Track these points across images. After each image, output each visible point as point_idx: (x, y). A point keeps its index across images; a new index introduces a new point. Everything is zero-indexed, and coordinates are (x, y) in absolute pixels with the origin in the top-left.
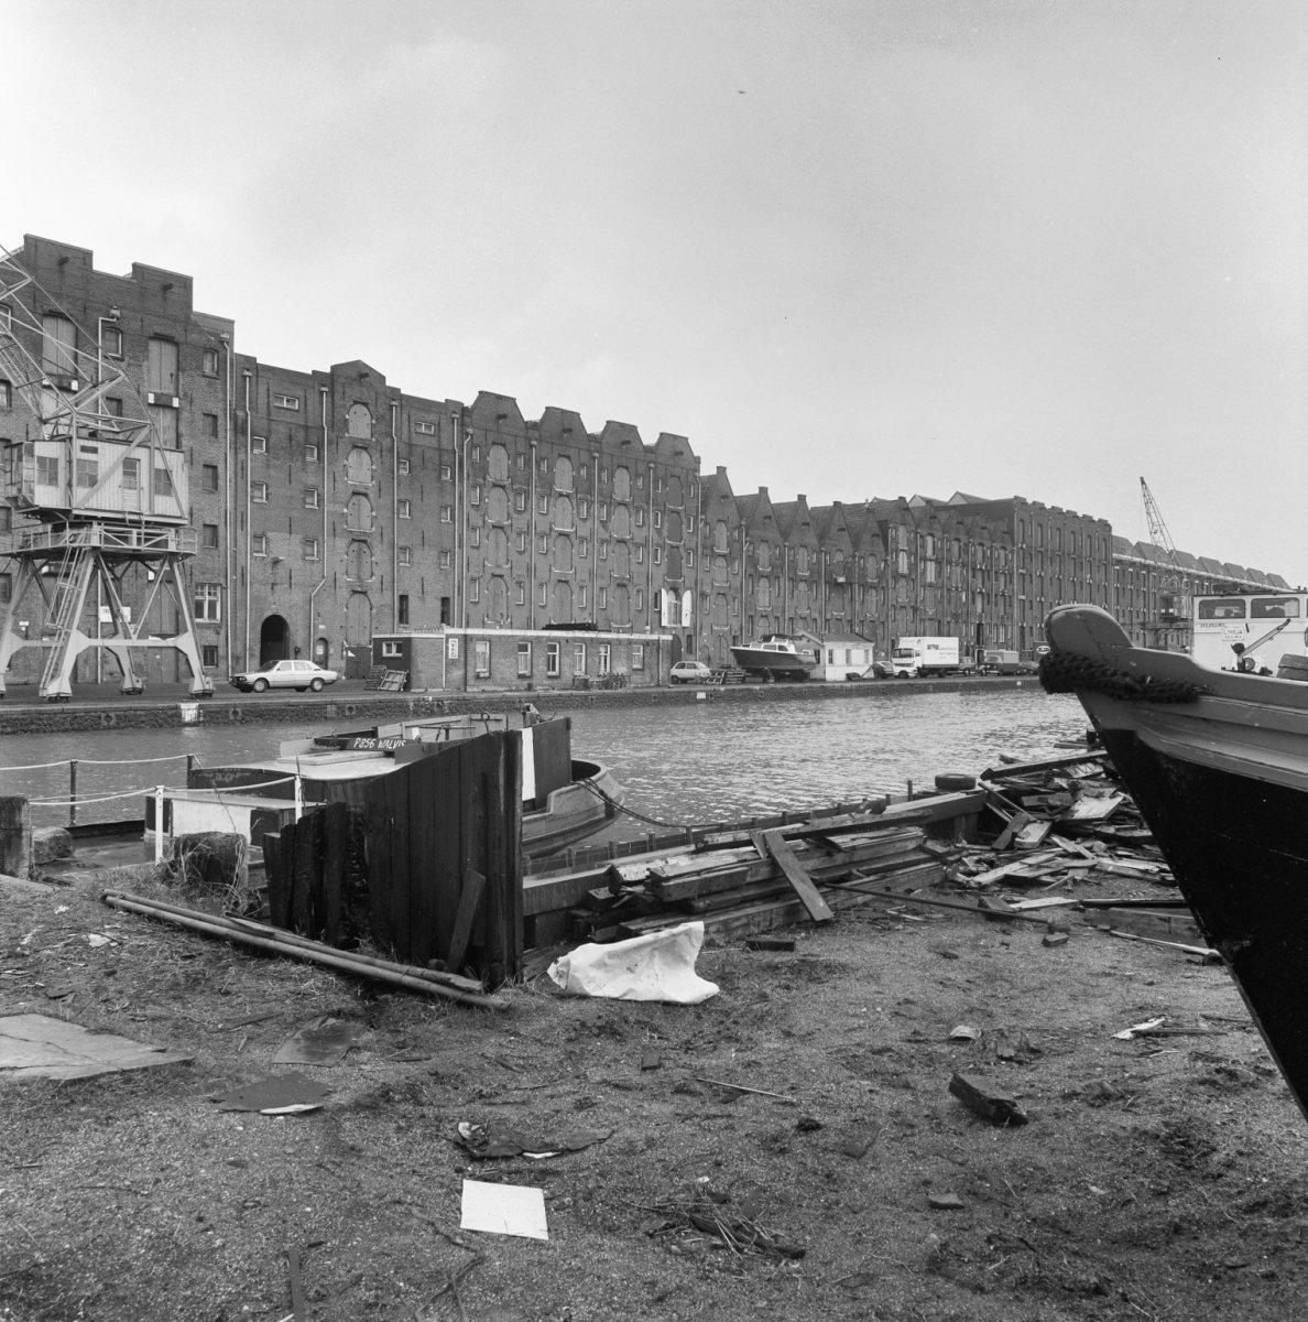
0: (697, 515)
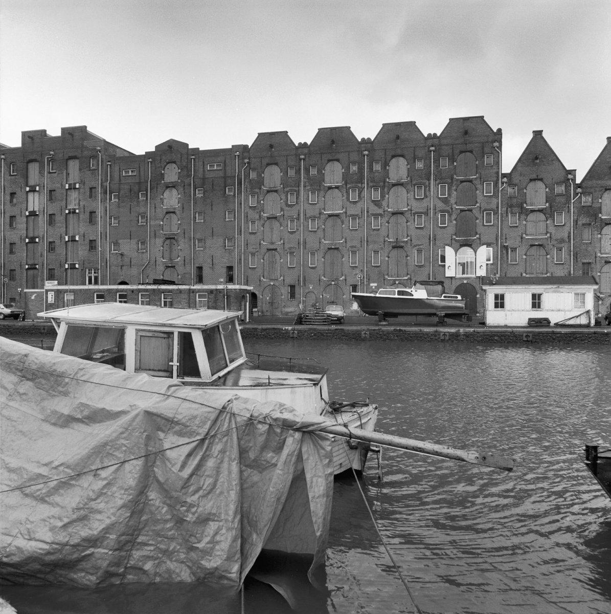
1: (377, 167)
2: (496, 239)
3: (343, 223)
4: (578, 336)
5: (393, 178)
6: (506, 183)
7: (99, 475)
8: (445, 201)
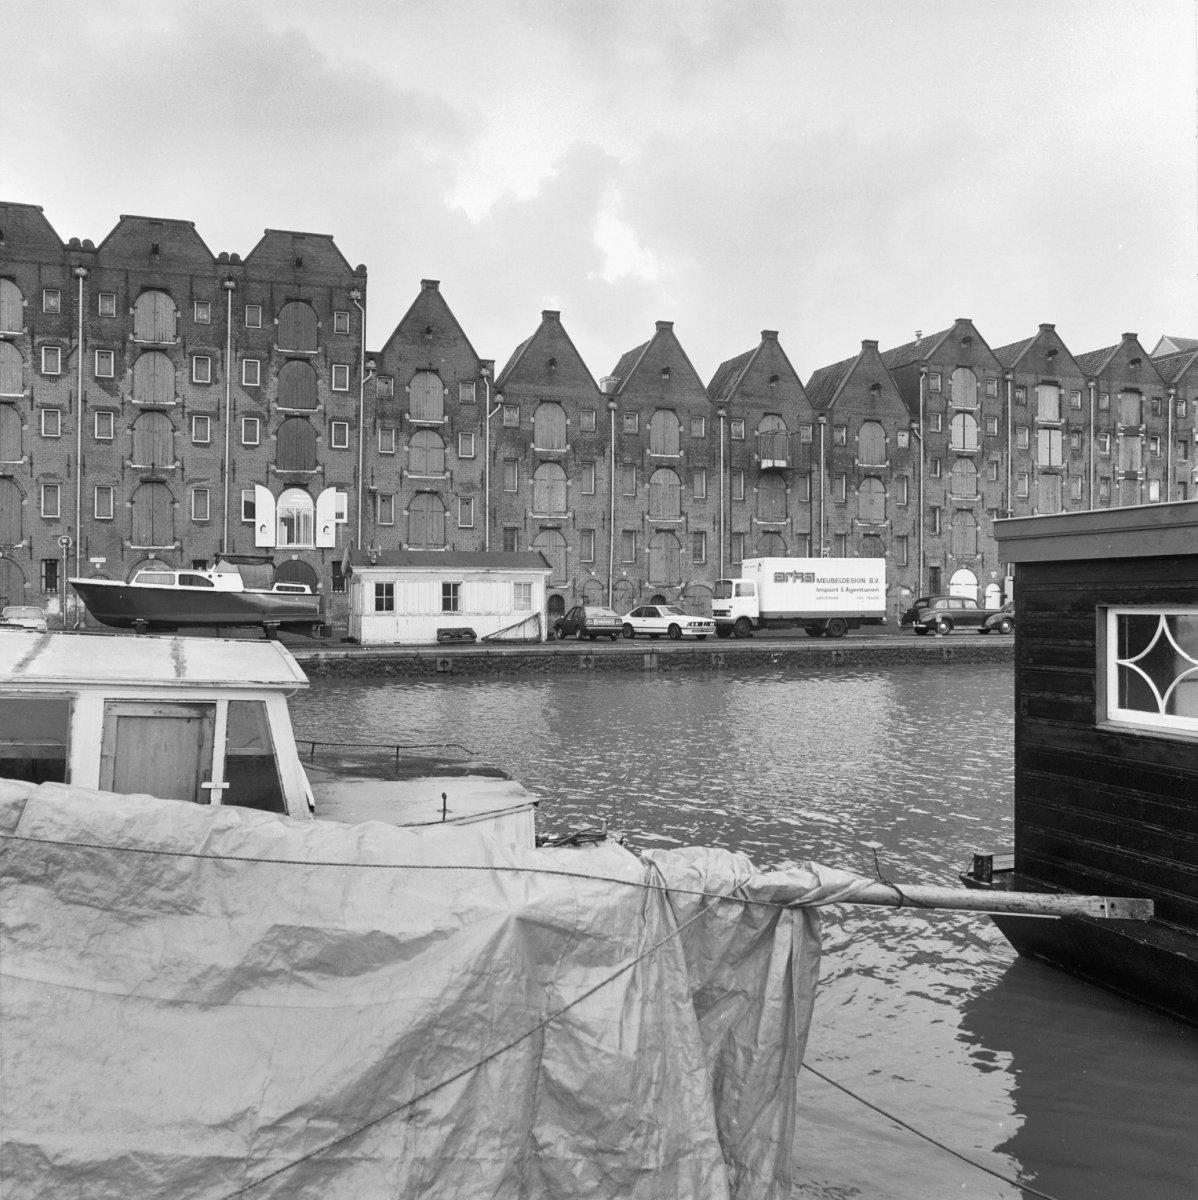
0: (358, 362)
1: (107, 307)
2: (355, 477)
3: (23, 420)
4: (529, 659)
5: (143, 334)
6: (374, 370)
7: (425, 1113)
8: (256, 394)
